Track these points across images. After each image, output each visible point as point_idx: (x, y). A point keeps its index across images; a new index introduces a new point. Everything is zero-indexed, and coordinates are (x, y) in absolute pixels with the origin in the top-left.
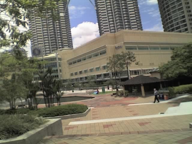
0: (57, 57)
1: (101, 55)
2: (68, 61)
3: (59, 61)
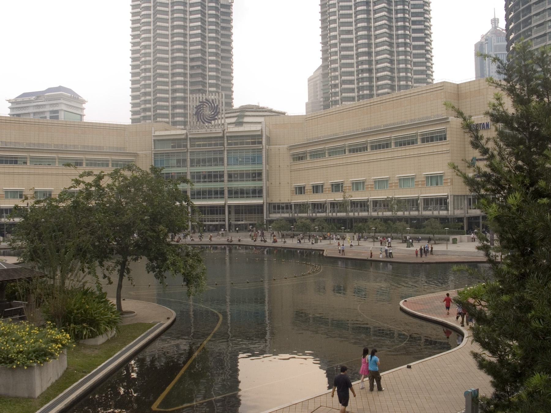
0: (264, 133)
2: (291, 148)
3: (267, 147)
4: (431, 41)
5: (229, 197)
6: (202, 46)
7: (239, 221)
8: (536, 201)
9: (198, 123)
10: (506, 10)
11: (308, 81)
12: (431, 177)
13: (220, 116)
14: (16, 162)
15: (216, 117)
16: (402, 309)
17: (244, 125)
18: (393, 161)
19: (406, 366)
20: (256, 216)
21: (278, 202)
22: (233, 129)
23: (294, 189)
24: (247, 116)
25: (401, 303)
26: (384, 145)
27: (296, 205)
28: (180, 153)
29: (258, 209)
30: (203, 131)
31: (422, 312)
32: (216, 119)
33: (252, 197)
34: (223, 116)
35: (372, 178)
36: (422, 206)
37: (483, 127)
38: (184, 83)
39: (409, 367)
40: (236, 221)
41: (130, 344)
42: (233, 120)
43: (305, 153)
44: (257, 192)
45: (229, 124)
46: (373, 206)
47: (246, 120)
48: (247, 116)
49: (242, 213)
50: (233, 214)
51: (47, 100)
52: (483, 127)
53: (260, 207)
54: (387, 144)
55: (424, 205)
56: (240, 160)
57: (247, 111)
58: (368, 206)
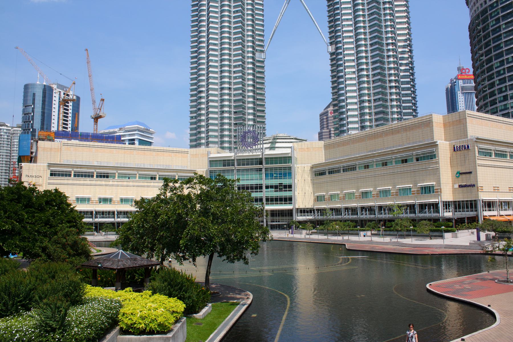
1: (345, 173)
4: (415, 84)
5: (266, 204)
6: (243, 91)
7: (274, 222)
8: (288, 222)
9: (243, 148)
10: (472, 60)
11: (320, 116)
12: (425, 187)
13: (259, 142)
14: (107, 177)
15: (257, 143)
16: (428, 291)
17: (276, 149)
18: (394, 175)
19: (460, 339)
20: (287, 218)
21: (304, 207)
22: (268, 152)
23: (316, 198)
24: (278, 142)
25: (428, 286)
26: (353, 168)
27: (318, 210)
28: (229, 170)
29: (290, 213)
30: (251, 154)
31: (448, 294)
32: (257, 145)
33: (275, 204)
34: (261, 142)
35: (419, 185)
36: (418, 210)
37: (464, 148)
38: (230, 118)
39: (463, 340)
40: (271, 222)
41: (228, 318)
42: (268, 145)
43: (324, 170)
44: (289, 200)
45: (266, 148)
46: (379, 210)
47: (277, 145)
48: (278, 142)
49: (276, 216)
50: (269, 217)
51: (126, 131)
52: (465, 148)
53: (291, 211)
54: (368, 165)
55: (420, 209)
56: (275, 175)
57: (278, 139)
58: (374, 211)
